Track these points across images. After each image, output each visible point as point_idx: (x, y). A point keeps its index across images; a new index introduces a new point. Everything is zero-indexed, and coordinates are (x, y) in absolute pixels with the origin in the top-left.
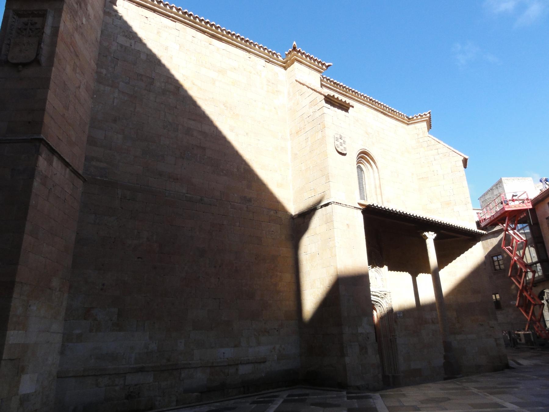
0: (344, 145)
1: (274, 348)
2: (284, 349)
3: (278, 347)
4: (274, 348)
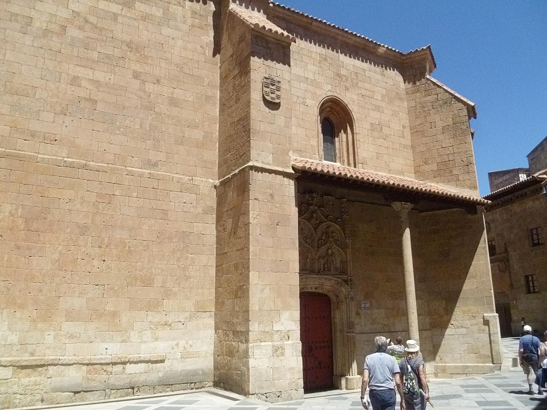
0: (277, 93)
1: (177, 345)
2: (191, 346)
3: (182, 343)
4: (177, 345)
